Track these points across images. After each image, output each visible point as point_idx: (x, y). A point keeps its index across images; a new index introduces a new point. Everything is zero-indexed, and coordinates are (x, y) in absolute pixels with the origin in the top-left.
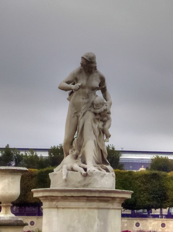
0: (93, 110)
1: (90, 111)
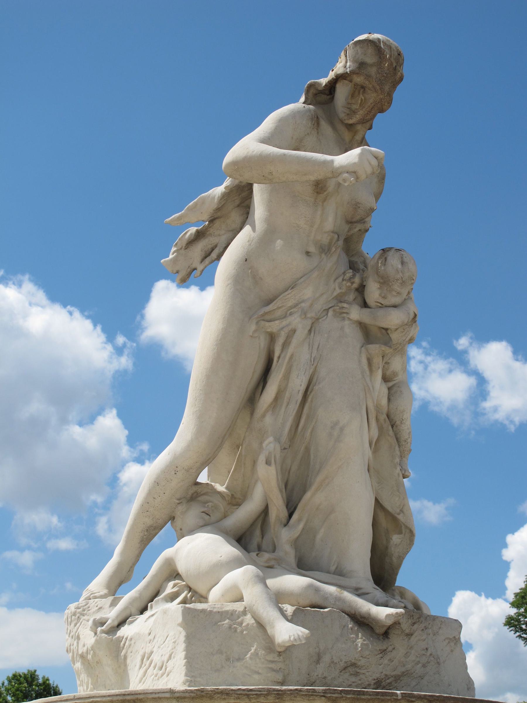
0: (356, 313)
1: (341, 314)
